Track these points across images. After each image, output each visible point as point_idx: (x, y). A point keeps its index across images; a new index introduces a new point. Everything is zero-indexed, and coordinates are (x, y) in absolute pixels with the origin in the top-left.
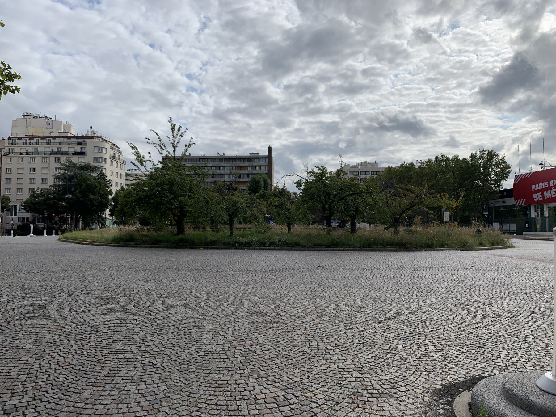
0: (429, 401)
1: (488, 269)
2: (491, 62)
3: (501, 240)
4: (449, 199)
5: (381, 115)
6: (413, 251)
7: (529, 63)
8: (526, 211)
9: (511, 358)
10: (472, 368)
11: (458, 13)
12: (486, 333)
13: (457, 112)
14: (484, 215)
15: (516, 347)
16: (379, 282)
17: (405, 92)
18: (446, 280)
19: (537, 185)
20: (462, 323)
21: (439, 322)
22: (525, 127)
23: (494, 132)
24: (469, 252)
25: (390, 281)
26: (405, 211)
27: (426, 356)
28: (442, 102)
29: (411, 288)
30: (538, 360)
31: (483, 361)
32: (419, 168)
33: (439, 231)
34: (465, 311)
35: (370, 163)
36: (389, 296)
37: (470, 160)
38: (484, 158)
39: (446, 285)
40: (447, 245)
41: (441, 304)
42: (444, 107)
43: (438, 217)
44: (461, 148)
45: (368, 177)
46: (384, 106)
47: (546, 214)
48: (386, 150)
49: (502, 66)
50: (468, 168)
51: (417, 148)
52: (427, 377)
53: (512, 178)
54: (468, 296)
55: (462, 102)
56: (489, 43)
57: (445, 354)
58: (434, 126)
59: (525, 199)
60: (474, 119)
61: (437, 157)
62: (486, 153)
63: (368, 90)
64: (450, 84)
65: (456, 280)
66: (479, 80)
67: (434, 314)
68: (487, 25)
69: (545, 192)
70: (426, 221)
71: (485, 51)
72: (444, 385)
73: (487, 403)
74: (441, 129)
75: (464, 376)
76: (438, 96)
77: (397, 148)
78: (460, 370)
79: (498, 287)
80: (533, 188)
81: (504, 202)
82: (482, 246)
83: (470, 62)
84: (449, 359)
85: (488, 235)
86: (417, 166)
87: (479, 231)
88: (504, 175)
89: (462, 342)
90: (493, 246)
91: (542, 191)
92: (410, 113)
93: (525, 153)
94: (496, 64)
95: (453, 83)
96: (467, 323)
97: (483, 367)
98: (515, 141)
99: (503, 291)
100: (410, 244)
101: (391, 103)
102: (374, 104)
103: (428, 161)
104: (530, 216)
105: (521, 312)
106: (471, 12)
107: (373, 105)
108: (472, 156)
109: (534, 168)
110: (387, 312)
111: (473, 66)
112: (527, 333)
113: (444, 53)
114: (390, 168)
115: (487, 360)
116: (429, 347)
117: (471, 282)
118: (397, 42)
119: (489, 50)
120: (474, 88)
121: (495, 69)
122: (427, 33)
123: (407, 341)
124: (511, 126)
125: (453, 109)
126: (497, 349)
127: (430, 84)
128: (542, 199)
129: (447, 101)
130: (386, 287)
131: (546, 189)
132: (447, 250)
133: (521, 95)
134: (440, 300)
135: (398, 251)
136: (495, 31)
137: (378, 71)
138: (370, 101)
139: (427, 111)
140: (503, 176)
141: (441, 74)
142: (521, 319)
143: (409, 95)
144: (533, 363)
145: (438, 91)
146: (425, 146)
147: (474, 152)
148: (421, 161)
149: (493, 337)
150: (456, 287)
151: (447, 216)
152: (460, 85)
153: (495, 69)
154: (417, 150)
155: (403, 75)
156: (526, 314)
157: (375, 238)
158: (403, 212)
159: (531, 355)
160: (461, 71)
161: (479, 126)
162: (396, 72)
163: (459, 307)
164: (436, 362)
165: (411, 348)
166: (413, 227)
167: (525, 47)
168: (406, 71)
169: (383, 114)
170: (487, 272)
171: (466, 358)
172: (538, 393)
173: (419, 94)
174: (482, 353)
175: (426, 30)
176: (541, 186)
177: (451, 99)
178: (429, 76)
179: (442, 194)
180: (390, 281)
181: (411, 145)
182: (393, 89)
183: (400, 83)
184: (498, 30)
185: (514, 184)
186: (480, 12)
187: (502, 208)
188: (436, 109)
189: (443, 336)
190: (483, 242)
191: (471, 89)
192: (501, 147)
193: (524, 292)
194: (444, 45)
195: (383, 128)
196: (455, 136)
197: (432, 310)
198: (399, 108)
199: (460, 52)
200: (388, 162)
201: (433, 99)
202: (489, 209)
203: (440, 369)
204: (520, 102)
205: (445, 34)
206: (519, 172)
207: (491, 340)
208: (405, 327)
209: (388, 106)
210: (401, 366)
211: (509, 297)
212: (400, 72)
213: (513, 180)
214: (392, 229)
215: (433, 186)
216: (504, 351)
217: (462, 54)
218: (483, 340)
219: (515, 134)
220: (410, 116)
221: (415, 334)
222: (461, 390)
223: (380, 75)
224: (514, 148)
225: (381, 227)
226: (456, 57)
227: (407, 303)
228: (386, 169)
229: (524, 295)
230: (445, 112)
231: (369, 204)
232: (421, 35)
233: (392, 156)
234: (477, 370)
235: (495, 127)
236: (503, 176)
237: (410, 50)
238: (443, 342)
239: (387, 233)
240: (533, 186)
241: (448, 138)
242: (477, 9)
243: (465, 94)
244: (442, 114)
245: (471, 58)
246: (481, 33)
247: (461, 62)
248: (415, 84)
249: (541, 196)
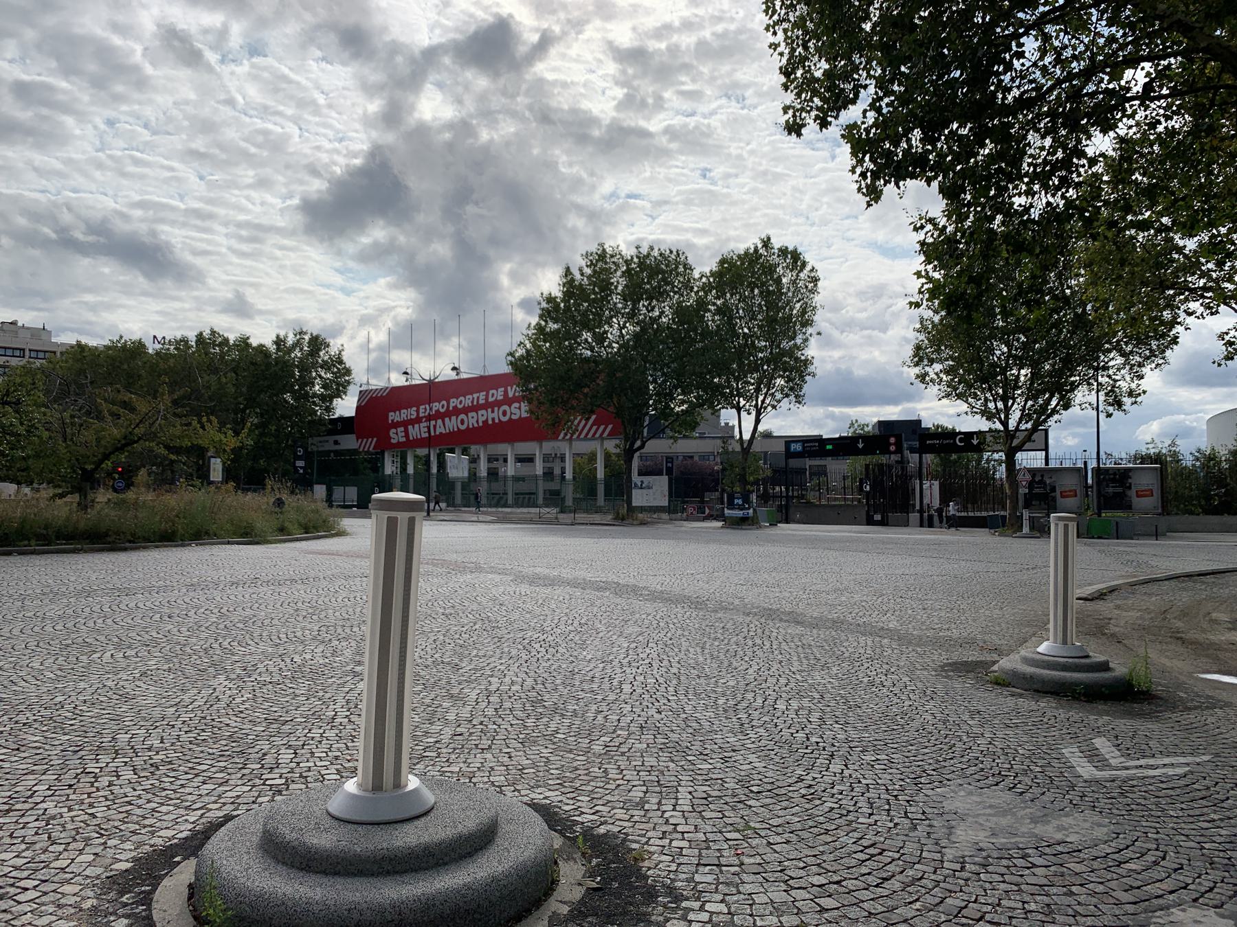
0: (94, 908)
1: (288, 583)
2: (327, 151)
3: (324, 522)
4: (220, 431)
5: (65, 210)
6: (125, 549)
7: (396, 171)
8: (376, 463)
9: (298, 763)
10: (214, 802)
11: (262, 23)
12: (259, 720)
13: (253, 240)
14: (295, 468)
15: (313, 738)
16: (16, 632)
17: (131, 169)
18: (191, 613)
19: (398, 413)
20: (211, 706)
21: (157, 713)
22: (384, 298)
23: (326, 297)
24: (255, 547)
25: (49, 629)
26: (111, 453)
27: (107, 800)
28: (221, 211)
29: (102, 638)
30: (349, 758)
31: (240, 782)
32: (158, 353)
33: (191, 502)
34: (222, 678)
35: (28, 328)
36: (36, 665)
37: (273, 348)
38: (301, 350)
39: (191, 625)
40: (207, 533)
41: (170, 670)
42: (226, 224)
43: (198, 470)
44: (259, 319)
45: (14, 362)
46: (75, 191)
47: (410, 470)
48: (75, 300)
49: (347, 165)
50: (268, 365)
51: (159, 308)
52: (99, 850)
53: (353, 396)
54: (236, 644)
55: (265, 221)
56: (325, 111)
57: (157, 785)
58: (199, 262)
59: (610, 427)
60: (288, 263)
61: (201, 334)
62: (307, 337)
63: (30, 139)
64: (241, 176)
65: (216, 611)
66: (301, 182)
67: (148, 696)
68: (323, 70)
69: (410, 427)
70: (165, 479)
71: (317, 124)
72: (140, 858)
73: (224, 875)
74: (216, 272)
75: (190, 826)
76: (212, 195)
77: (106, 299)
78: (184, 813)
79: (300, 618)
80: (390, 418)
81: (336, 443)
82: (283, 533)
83: (286, 138)
84: (164, 794)
85: (299, 510)
86: (152, 348)
87: (280, 503)
88: (338, 387)
89: (203, 748)
90: (306, 533)
91: (405, 424)
92: (142, 220)
93: (380, 348)
94: (336, 157)
95: (248, 175)
96: (223, 704)
97: (238, 797)
98: (365, 321)
99: (309, 626)
100: (117, 533)
101: (93, 187)
102: (48, 180)
103: (181, 341)
104: (383, 472)
105: (335, 665)
106: (291, 28)
107: (44, 182)
108: (279, 342)
109: (396, 380)
110: (22, 707)
111: (291, 150)
112: (338, 705)
113: (231, 102)
114: (80, 347)
115: (247, 779)
116: (118, 777)
117: (249, 612)
118: (117, 41)
119: (325, 125)
120: (291, 197)
121: (334, 168)
122: (192, 45)
123: (65, 771)
124: (360, 290)
125: (244, 233)
126: (273, 751)
127: (196, 164)
128: (404, 439)
129: (231, 212)
130: (32, 644)
132: (207, 544)
133: (377, 233)
134: (168, 661)
135: (86, 552)
136: (337, 89)
137: (61, 97)
138: (36, 169)
139: (184, 225)
140: (338, 389)
141: (220, 146)
142: (333, 680)
143: (142, 177)
144: (339, 766)
145: (212, 185)
146: (177, 305)
147: (282, 334)
148: (164, 338)
149: (272, 726)
150: (213, 628)
151: (216, 469)
152: (263, 183)
153: (334, 168)
154: (157, 312)
155: (128, 127)
156: (344, 669)
157: (24, 521)
158: (106, 457)
159: (338, 749)
160: (265, 154)
161: (298, 278)
162: (110, 113)
163: (212, 670)
164: (129, 808)
165: (70, 786)
166: (130, 495)
167: (389, 138)
168: (138, 118)
169: (69, 209)
170: (284, 589)
171: (204, 783)
172: (327, 826)
173: (167, 181)
174: (240, 766)
175: (191, 36)
176: (405, 414)
177: (241, 209)
178: (193, 146)
179: (204, 419)
180: (49, 629)
181: (143, 298)
182: (100, 154)
183: (122, 144)
184: (344, 88)
185: (358, 408)
186: (309, 38)
187: (332, 454)
188: (207, 224)
189: (162, 742)
190: (287, 524)
191: (286, 198)
192: (338, 330)
193: (349, 624)
194: (232, 85)
195: (67, 243)
196: (247, 294)
197: (145, 686)
198: (116, 203)
199: (265, 111)
200: (80, 332)
201: (201, 199)
202: (308, 456)
203: (137, 823)
204: (376, 244)
205: (233, 61)
206: (368, 383)
207: (266, 733)
208: (67, 737)
209: (85, 192)
210: (36, 838)
211: (319, 638)
212: (123, 118)
213: (356, 399)
214: (76, 498)
215: (183, 397)
216: (288, 751)
217: (269, 118)
218: (250, 737)
219: (366, 308)
220: (143, 228)
221: (90, 751)
222: (177, 859)
223: (67, 109)
224: (362, 336)
225: (46, 492)
226: (255, 120)
227: (83, 677)
228: (72, 347)
229: (348, 630)
230: (226, 235)
231: (12, 434)
232: (176, 43)
233: (91, 317)
234: (224, 804)
235: (329, 286)
236: (338, 389)
237: (149, 70)
238: (157, 759)
239: (63, 509)
240: (391, 414)
241: (230, 296)
242: (302, 29)
243: (271, 205)
244: (221, 239)
245: (288, 130)
246: (309, 84)
247: (265, 133)
248: (159, 155)
249: (403, 434)
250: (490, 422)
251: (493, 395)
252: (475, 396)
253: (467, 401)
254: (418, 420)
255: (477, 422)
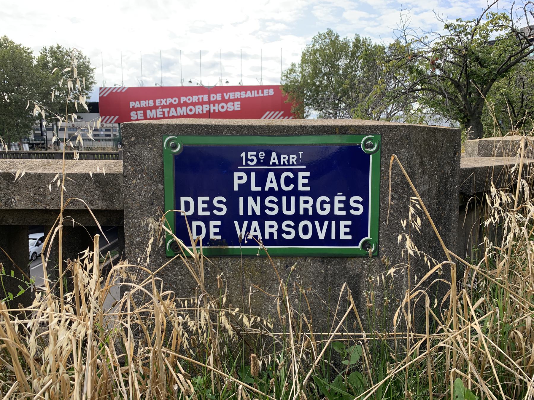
59: (117, 117)
131: (151, 109)
176: (143, 104)
240: (131, 103)
250: (212, 111)
251: (213, 97)
252: (200, 97)
253: (195, 99)
254: (155, 107)
255: (202, 111)
